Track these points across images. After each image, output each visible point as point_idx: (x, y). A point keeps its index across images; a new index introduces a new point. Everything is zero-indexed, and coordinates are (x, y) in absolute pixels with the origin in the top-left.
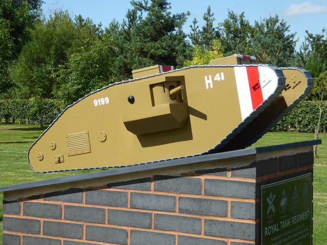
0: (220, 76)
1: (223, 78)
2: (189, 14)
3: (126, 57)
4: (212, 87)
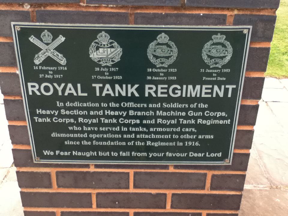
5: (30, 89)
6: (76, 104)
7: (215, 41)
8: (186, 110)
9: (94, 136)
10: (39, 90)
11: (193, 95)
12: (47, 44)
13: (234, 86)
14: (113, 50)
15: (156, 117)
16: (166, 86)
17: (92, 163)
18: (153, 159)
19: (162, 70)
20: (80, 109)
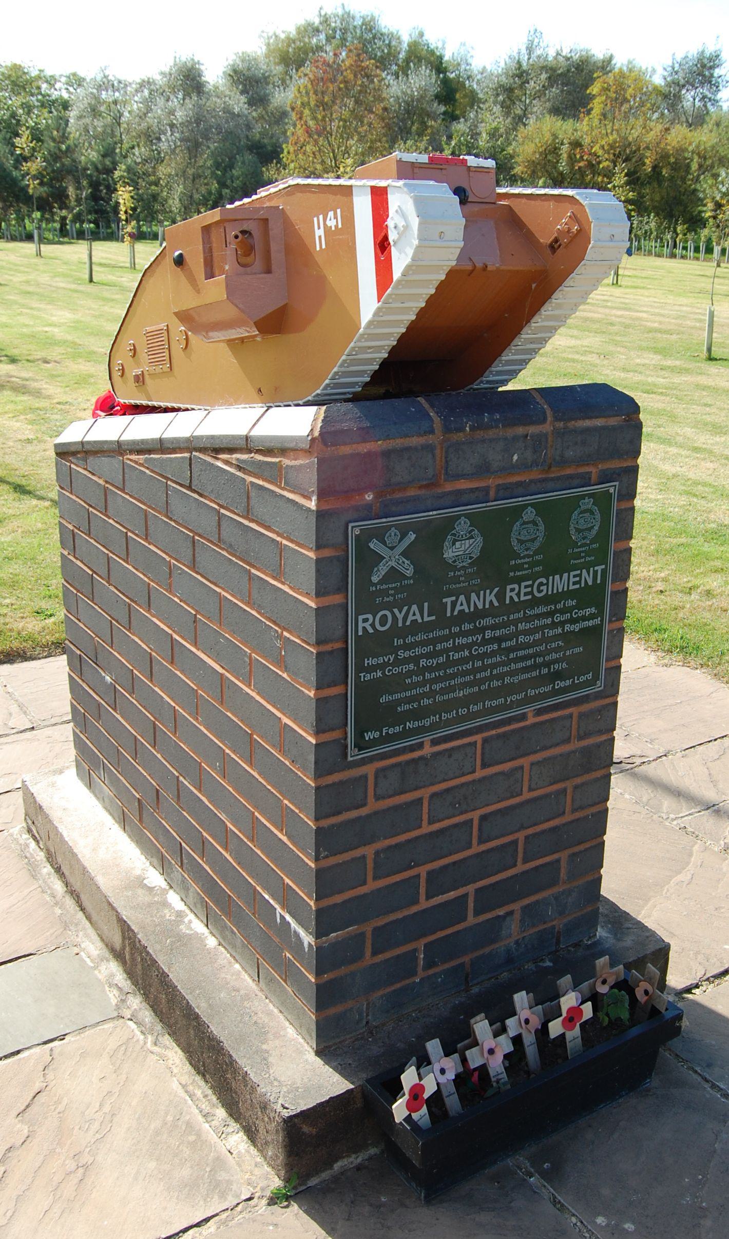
5: (361, 625)
6: (420, 637)
7: (583, 507)
8: (551, 614)
9: (437, 687)
10: (373, 625)
11: (480, 607)
12: (392, 548)
13: (603, 567)
14: (472, 541)
15: (517, 634)
16: (530, 582)
17: (529, 710)
18: (564, 690)
19: (527, 560)
20: (423, 643)
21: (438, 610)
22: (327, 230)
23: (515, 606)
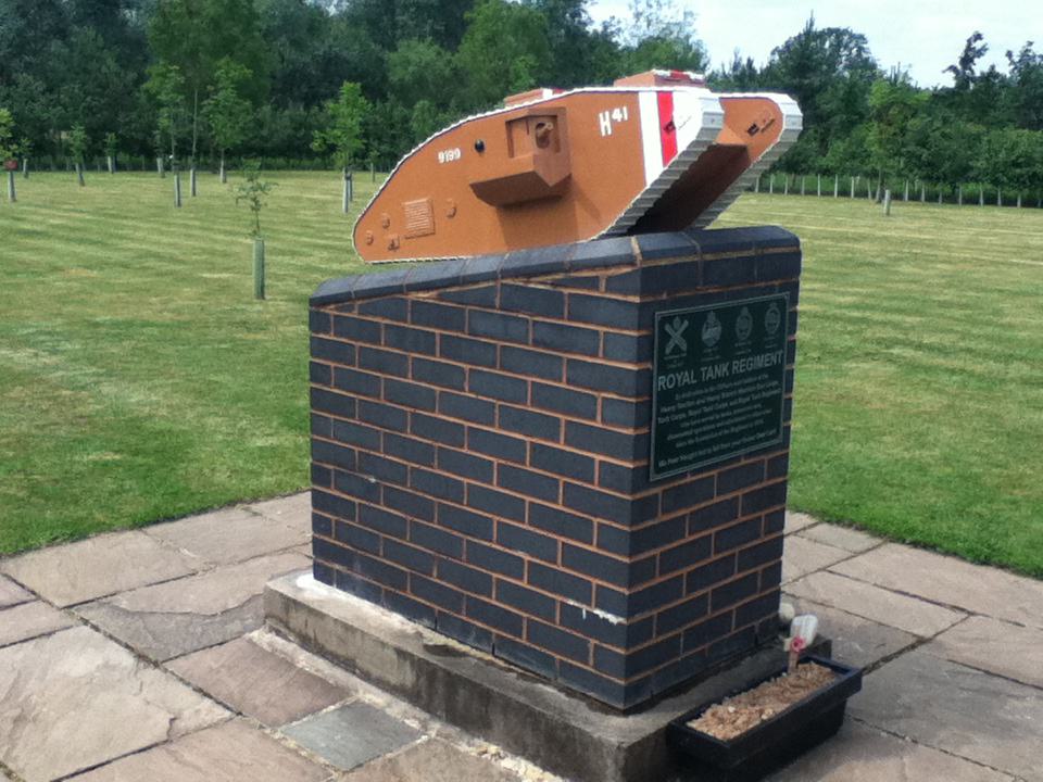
0: (622, 111)
1: (626, 118)
2: (1031, 44)
3: (945, 121)
4: (609, 132)
21: (698, 376)
22: (613, 122)
23: (711, 382)
